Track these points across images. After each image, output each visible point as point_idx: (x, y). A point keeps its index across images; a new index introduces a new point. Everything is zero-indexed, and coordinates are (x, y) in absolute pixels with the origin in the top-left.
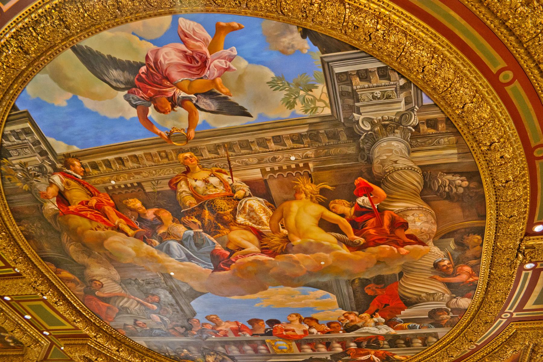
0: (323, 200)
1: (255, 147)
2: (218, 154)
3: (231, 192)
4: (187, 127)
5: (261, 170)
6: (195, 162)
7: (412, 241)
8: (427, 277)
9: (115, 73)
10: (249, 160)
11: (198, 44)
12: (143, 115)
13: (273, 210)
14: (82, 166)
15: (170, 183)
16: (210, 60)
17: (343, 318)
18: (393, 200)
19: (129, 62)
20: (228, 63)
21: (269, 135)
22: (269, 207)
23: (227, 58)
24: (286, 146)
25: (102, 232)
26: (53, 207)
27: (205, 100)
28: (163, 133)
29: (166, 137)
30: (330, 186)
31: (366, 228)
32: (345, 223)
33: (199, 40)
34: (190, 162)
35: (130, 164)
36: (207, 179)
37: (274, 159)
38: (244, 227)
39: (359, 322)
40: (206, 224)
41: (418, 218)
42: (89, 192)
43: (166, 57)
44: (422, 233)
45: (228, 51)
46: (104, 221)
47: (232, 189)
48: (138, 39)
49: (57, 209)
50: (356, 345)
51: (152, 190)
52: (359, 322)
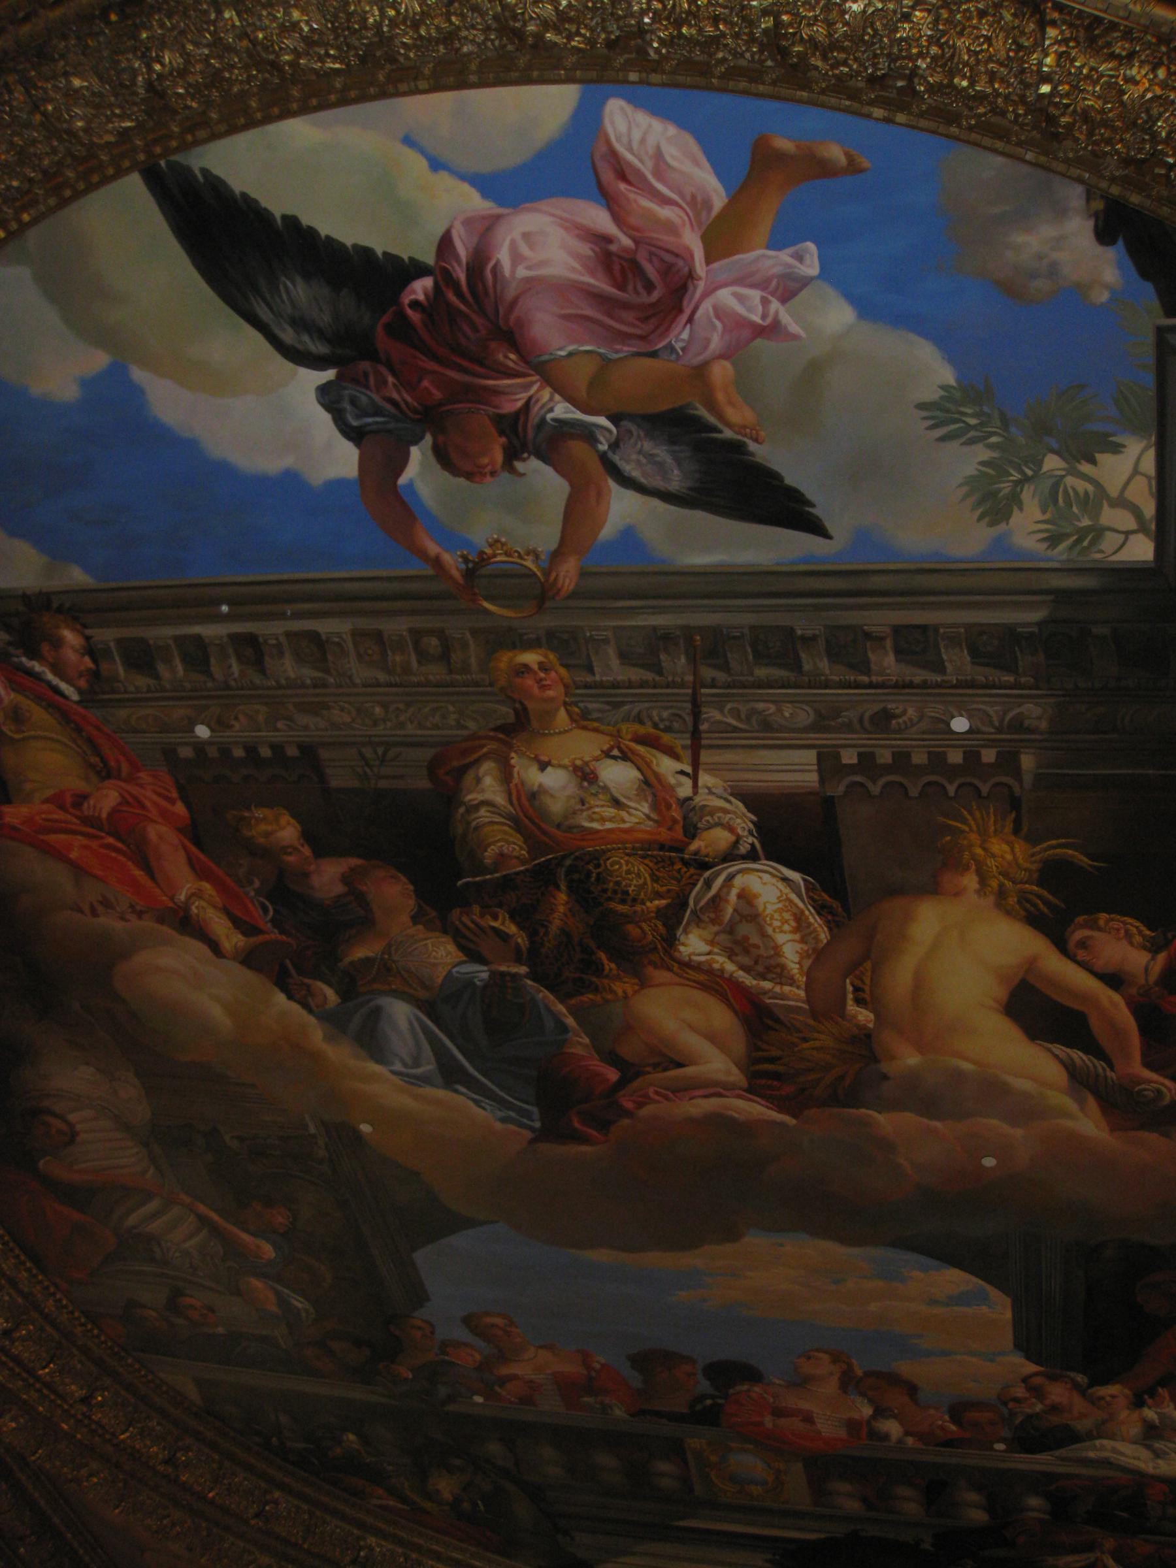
0: (1046, 910)
4: (553, 545)
11: (666, 212)
14: (90, 650)
15: (432, 767)
16: (701, 286)
19: (366, 253)
20: (775, 305)
21: (880, 620)
25: (119, 925)
27: (648, 446)
28: (447, 558)
30: (1088, 856)
37: (882, 721)
38: (701, 977)
42: (94, 760)
45: (785, 256)
48: (424, 163)
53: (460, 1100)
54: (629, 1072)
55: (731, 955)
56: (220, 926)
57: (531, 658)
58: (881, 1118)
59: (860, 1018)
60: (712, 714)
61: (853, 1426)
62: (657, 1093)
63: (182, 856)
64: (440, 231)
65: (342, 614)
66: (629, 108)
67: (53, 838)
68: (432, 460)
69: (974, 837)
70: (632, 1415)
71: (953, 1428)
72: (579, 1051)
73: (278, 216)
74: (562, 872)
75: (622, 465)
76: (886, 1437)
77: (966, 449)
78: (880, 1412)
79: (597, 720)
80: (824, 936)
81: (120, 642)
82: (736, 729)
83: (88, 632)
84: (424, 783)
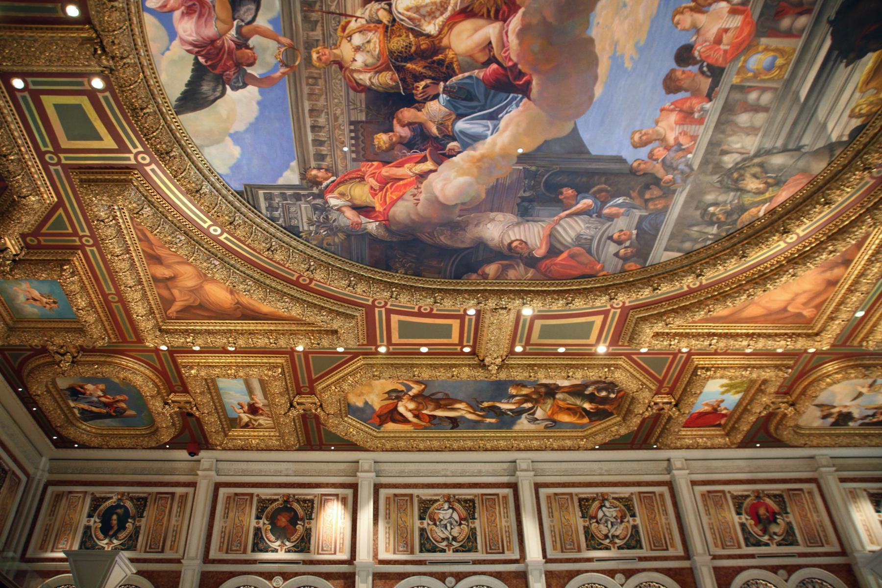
3: (378, 25)
4: (276, 43)
6: (327, 51)
12: (254, 80)
19: (193, 70)
38: (446, 29)
47: (374, 23)
54: (493, 60)
62: (505, 53)
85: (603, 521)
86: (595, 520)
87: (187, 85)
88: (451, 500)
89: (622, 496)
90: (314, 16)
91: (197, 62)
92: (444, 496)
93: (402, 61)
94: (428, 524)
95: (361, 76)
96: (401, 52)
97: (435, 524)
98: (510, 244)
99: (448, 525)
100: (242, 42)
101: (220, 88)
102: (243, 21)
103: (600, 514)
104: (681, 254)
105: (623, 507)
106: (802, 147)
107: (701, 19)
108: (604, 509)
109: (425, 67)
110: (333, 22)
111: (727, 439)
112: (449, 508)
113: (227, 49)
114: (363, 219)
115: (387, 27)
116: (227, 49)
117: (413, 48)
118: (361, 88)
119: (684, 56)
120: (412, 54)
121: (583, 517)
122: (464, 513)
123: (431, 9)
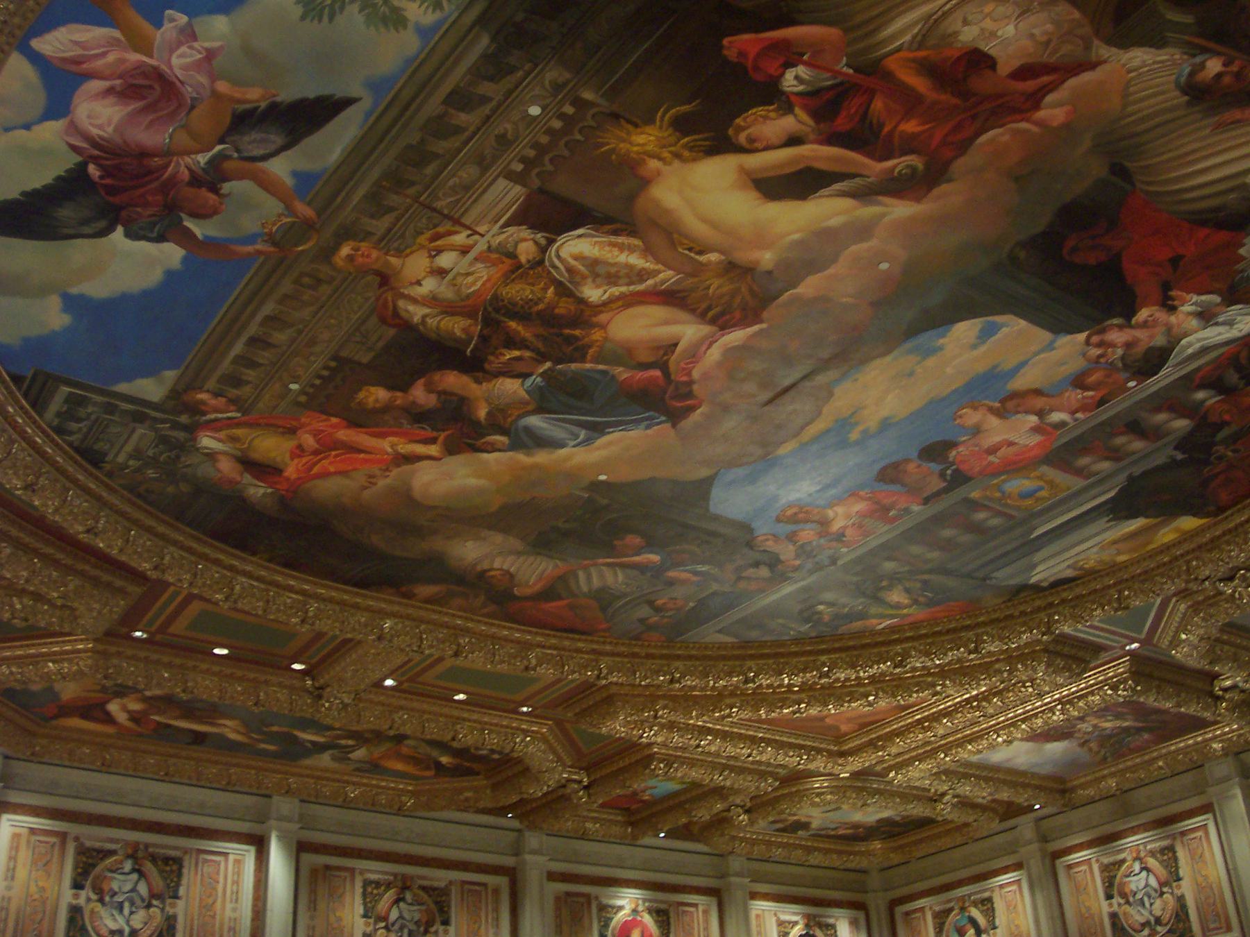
0: (707, 143)
1: (441, 146)
2: (391, 209)
3: (504, 259)
4: (282, 205)
5: (505, 177)
6: (375, 254)
7: (1045, 79)
8: (1207, 131)
9: (66, 212)
10: (460, 177)
11: (111, 58)
12: (186, 238)
13: (633, 233)
14: (217, 395)
15: (383, 320)
16: (164, 67)
17: (1095, 352)
18: (871, 27)
19: (59, 178)
20: (196, 45)
21: (433, 105)
22: (616, 233)
23: (182, 38)
24: (491, 99)
25: (388, 481)
26: (261, 491)
27: (246, 138)
28: (259, 247)
29: (272, 249)
30: (684, 104)
31: (886, 129)
32: (818, 153)
33: (102, 50)
34: (366, 260)
35: (280, 337)
36: (435, 265)
37: (504, 141)
38: (620, 303)
39: (1152, 337)
40: (540, 345)
41: (988, 20)
42: (281, 430)
43: (99, 122)
44: (1048, 42)
45: (167, 26)
46: (366, 461)
47: (500, 253)
48: (23, 132)
49: (269, 490)
50: (1212, 392)
51: (372, 354)
52: (1152, 337)
53: (614, 436)
54: (664, 367)
55: (616, 284)
56: (420, 449)
57: (345, 250)
58: (799, 290)
59: (713, 259)
60: (439, 204)
61: (1036, 430)
62: (687, 364)
63: (366, 437)
64: (66, 148)
65: (262, 303)
66: (39, 39)
67: (315, 470)
68: (197, 221)
69: (622, 145)
70: (924, 504)
71: (1091, 393)
72: (625, 376)
73: (18, 197)
74: (494, 315)
75: (251, 154)
76: (1063, 424)
77: (346, 12)
78: (1040, 414)
79: (406, 248)
80: (636, 242)
81: (218, 381)
82: (458, 201)
83: (206, 388)
84: (392, 332)
85: (396, 927)
86: (383, 924)
87: (24, 194)
88: (140, 854)
89: (436, 884)
90: (394, 199)
91: (81, 169)
92: (127, 843)
93: (504, 315)
94: (89, 900)
95: (411, 308)
96: (515, 305)
97: (101, 900)
98: (485, 571)
99: (126, 905)
100: (212, 178)
101: (102, 224)
102: (238, 151)
103: (394, 914)
104: (735, 640)
105: (432, 906)
106: (991, 579)
107: (994, 421)
108: (402, 904)
109: (537, 336)
110: (424, 220)
111: (630, 830)
112: (134, 870)
113: (166, 175)
114: (248, 478)
115: (520, 266)
116: (166, 175)
117: (541, 306)
118: (397, 321)
119: (935, 451)
120: (531, 314)
121: (365, 916)
122: (158, 883)
123: (617, 272)
